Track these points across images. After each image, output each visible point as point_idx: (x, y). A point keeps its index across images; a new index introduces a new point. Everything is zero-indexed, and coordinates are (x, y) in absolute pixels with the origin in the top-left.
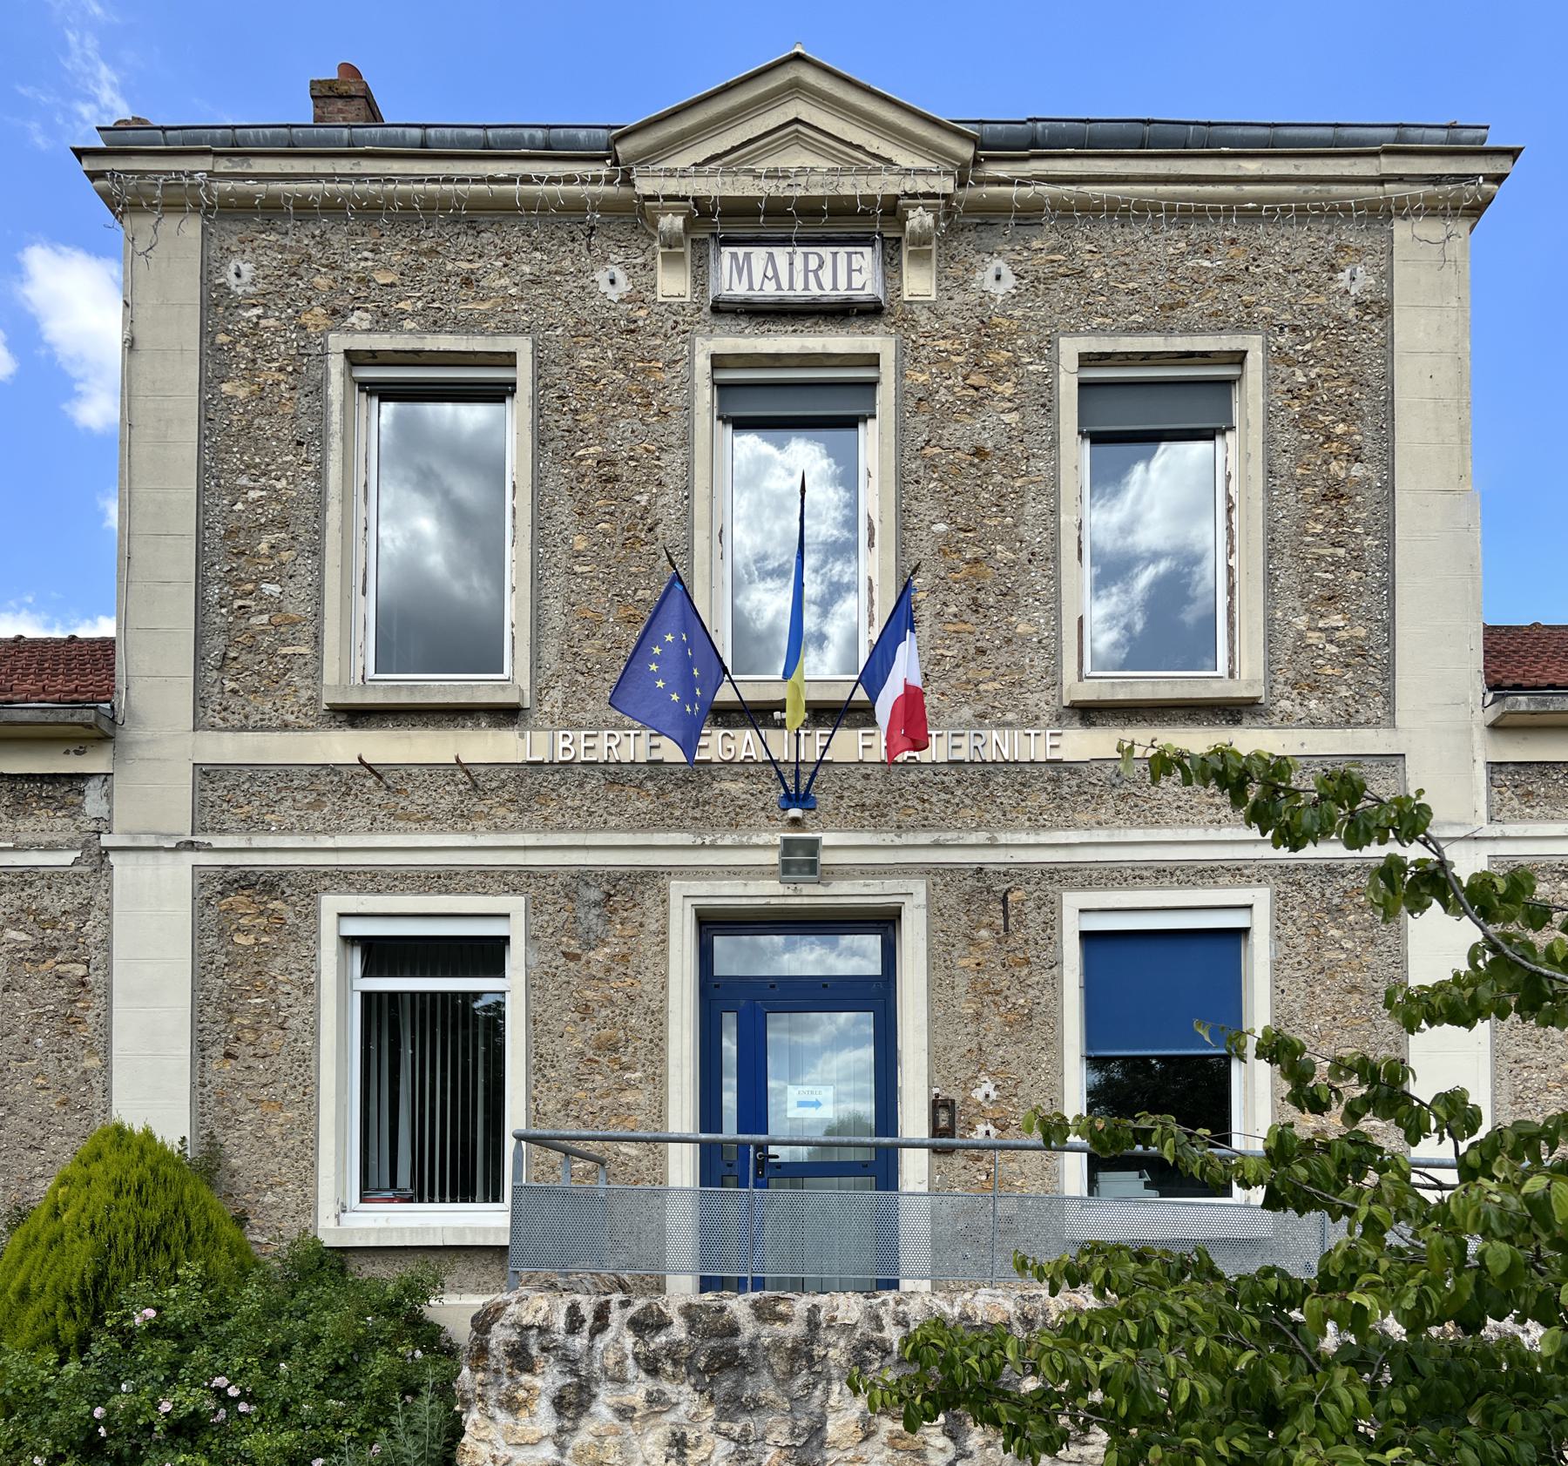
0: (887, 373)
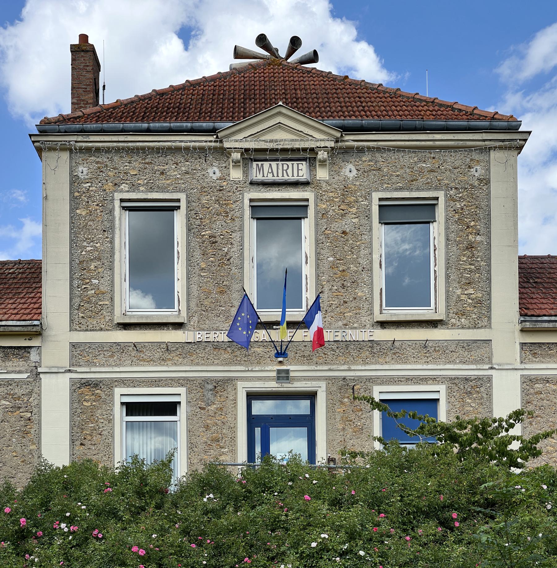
0: (311, 204)
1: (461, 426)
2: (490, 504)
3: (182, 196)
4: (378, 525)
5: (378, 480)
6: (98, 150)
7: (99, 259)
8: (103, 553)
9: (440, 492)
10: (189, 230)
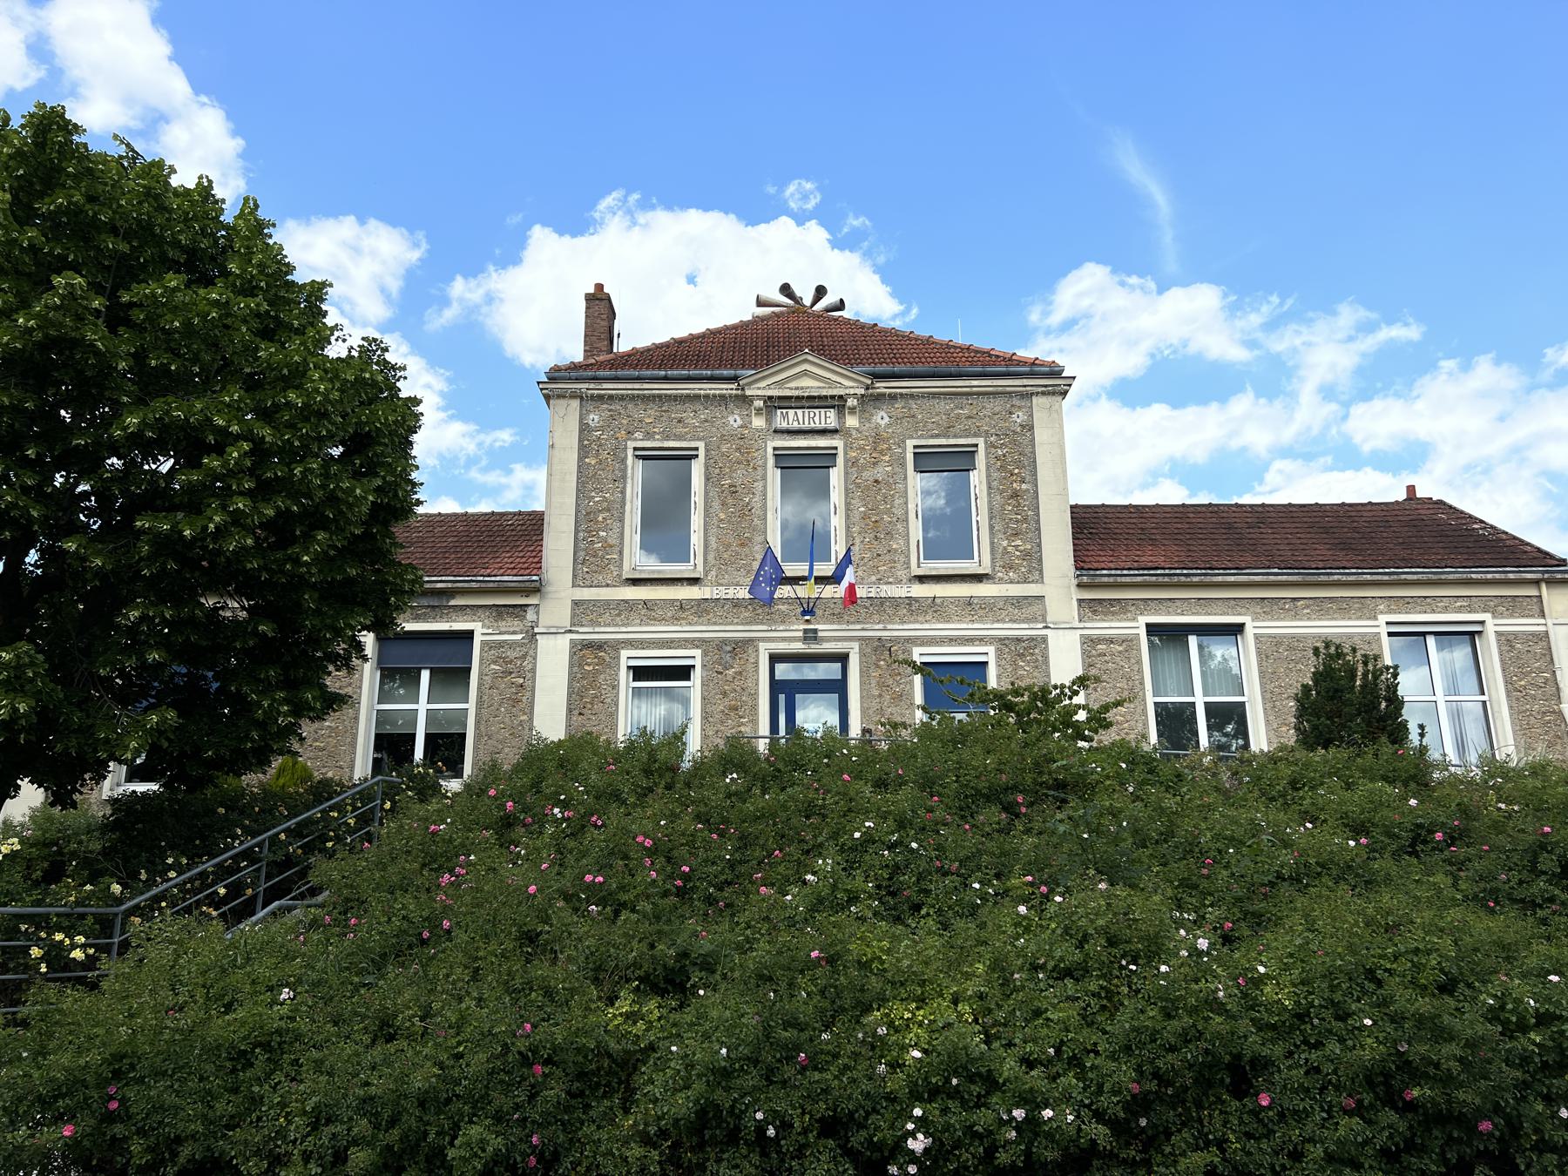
0: (841, 452)
1: (1017, 692)
2: (1061, 785)
3: (701, 445)
4: (930, 810)
5: (929, 756)
6: (611, 397)
7: (609, 510)
8: (603, 845)
9: (1001, 771)
10: (707, 479)
